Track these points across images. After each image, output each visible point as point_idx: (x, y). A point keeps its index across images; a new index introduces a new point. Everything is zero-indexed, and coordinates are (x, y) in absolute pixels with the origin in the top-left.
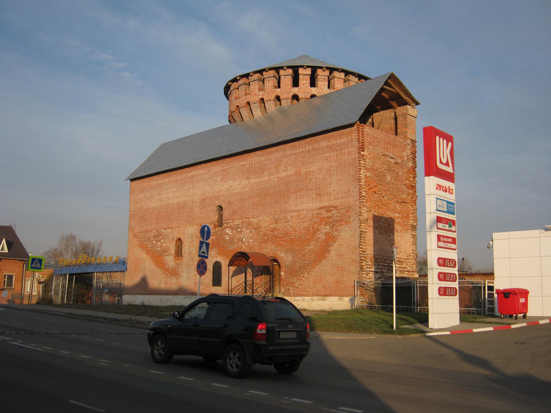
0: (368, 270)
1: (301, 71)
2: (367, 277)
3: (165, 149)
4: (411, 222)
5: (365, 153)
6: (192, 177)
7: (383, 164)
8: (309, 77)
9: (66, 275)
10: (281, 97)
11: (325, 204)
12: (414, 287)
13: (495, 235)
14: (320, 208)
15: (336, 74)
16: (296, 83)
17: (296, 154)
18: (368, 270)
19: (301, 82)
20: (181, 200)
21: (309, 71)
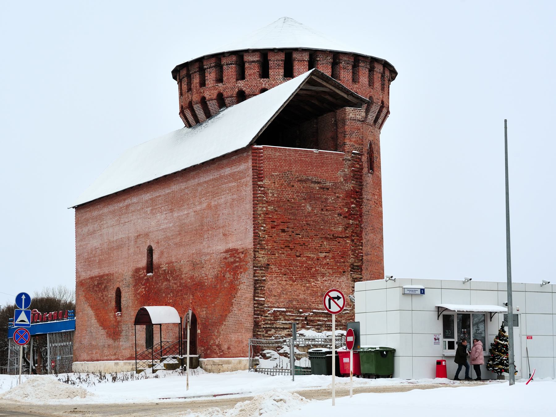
0: (268, 326)
1: (247, 58)
2: (267, 335)
4: (351, 260)
5: (266, 182)
6: (127, 206)
7: (298, 192)
10: (225, 95)
13: (145, 326)
16: (241, 76)
18: (268, 326)
19: (247, 72)
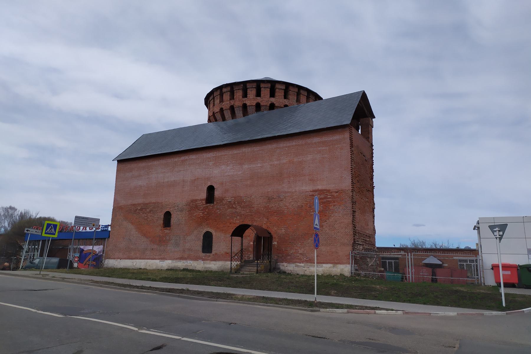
3: (147, 139)
6: (183, 161)
8: (283, 91)
9: (40, 241)
11: (320, 187)
12: (408, 259)
14: (314, 191)
15: (302, 91)
17: (289, 147)
19: (276, 94)
20: (172, 179)
21: (283, 87)
